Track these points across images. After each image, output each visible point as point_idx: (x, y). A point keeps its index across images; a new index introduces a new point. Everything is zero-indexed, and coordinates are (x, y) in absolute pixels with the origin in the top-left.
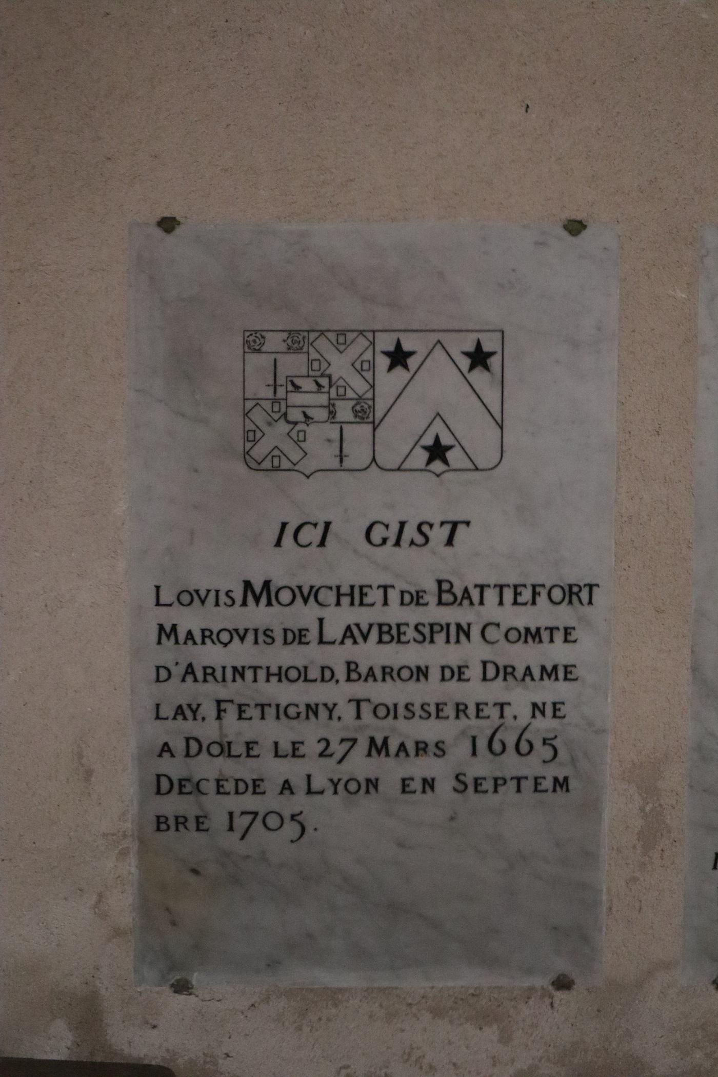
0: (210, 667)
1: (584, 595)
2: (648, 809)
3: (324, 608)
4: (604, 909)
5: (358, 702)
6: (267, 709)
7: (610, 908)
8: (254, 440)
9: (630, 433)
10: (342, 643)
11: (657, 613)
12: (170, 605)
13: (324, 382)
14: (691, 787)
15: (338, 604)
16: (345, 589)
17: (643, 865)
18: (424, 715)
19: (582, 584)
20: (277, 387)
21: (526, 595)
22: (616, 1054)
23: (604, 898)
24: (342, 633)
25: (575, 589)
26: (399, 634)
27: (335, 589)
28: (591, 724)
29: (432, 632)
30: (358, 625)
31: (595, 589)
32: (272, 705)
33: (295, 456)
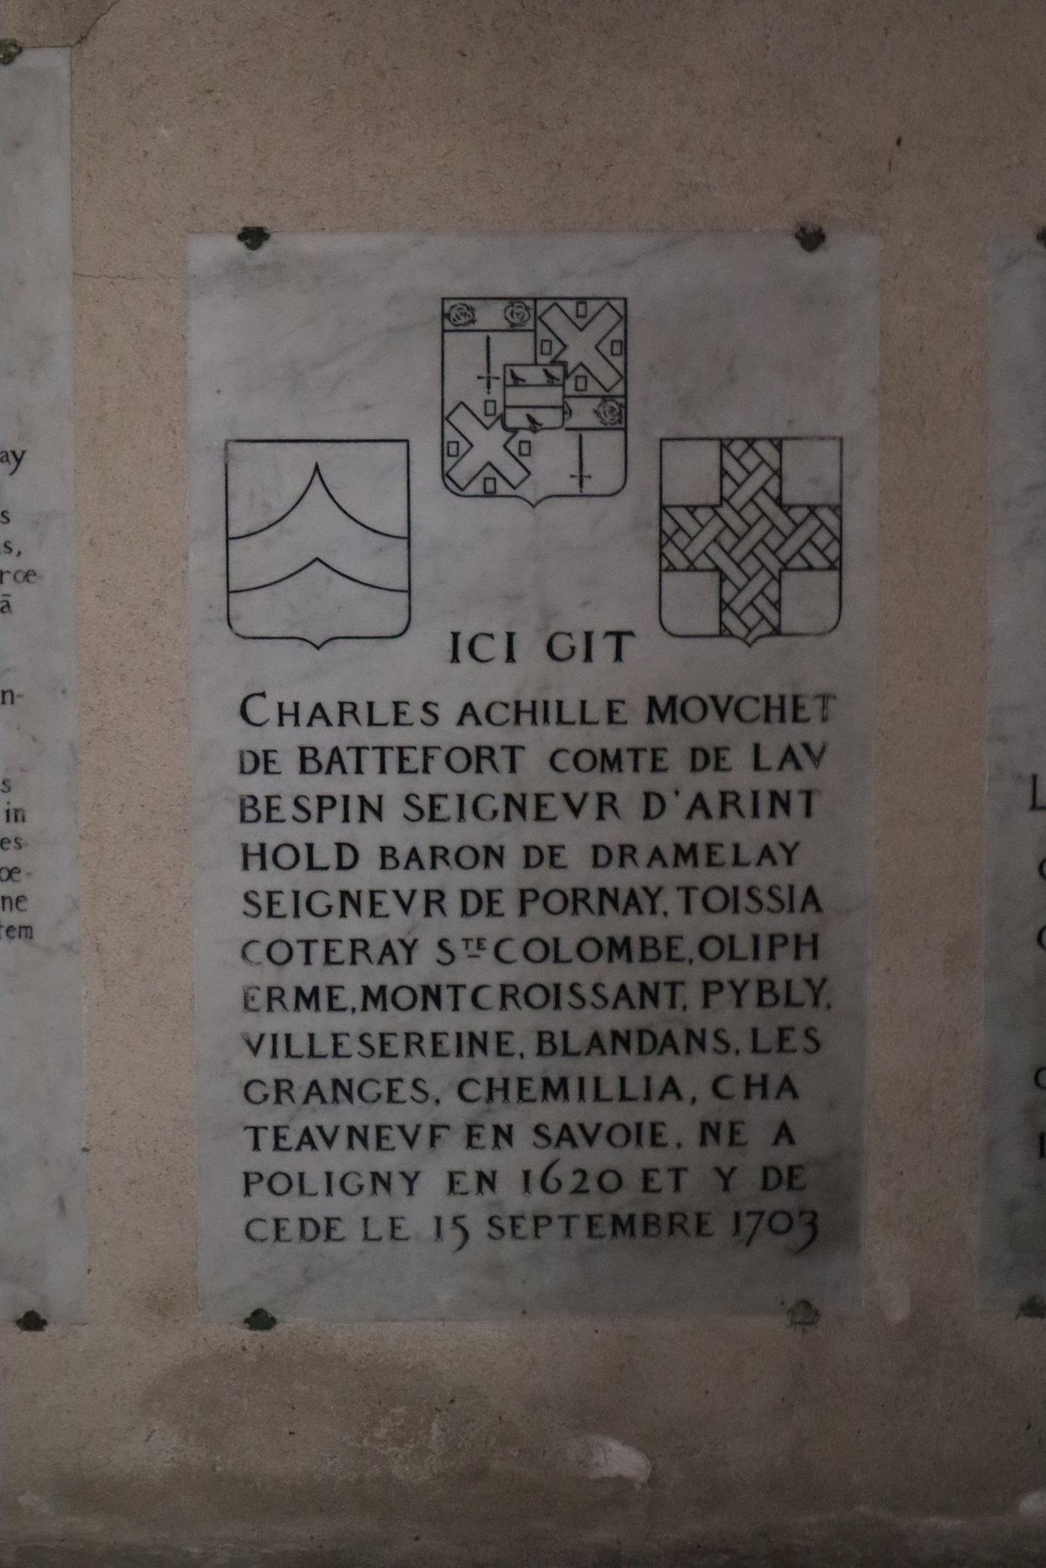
0: (389, 847)
5: (256, 1129)
8: (458, 455)
13: (557, 372)
18: (599, 1002)
20: (584, 479)
21: (416, 759)
26: (270, 808)
33: (515, 473)
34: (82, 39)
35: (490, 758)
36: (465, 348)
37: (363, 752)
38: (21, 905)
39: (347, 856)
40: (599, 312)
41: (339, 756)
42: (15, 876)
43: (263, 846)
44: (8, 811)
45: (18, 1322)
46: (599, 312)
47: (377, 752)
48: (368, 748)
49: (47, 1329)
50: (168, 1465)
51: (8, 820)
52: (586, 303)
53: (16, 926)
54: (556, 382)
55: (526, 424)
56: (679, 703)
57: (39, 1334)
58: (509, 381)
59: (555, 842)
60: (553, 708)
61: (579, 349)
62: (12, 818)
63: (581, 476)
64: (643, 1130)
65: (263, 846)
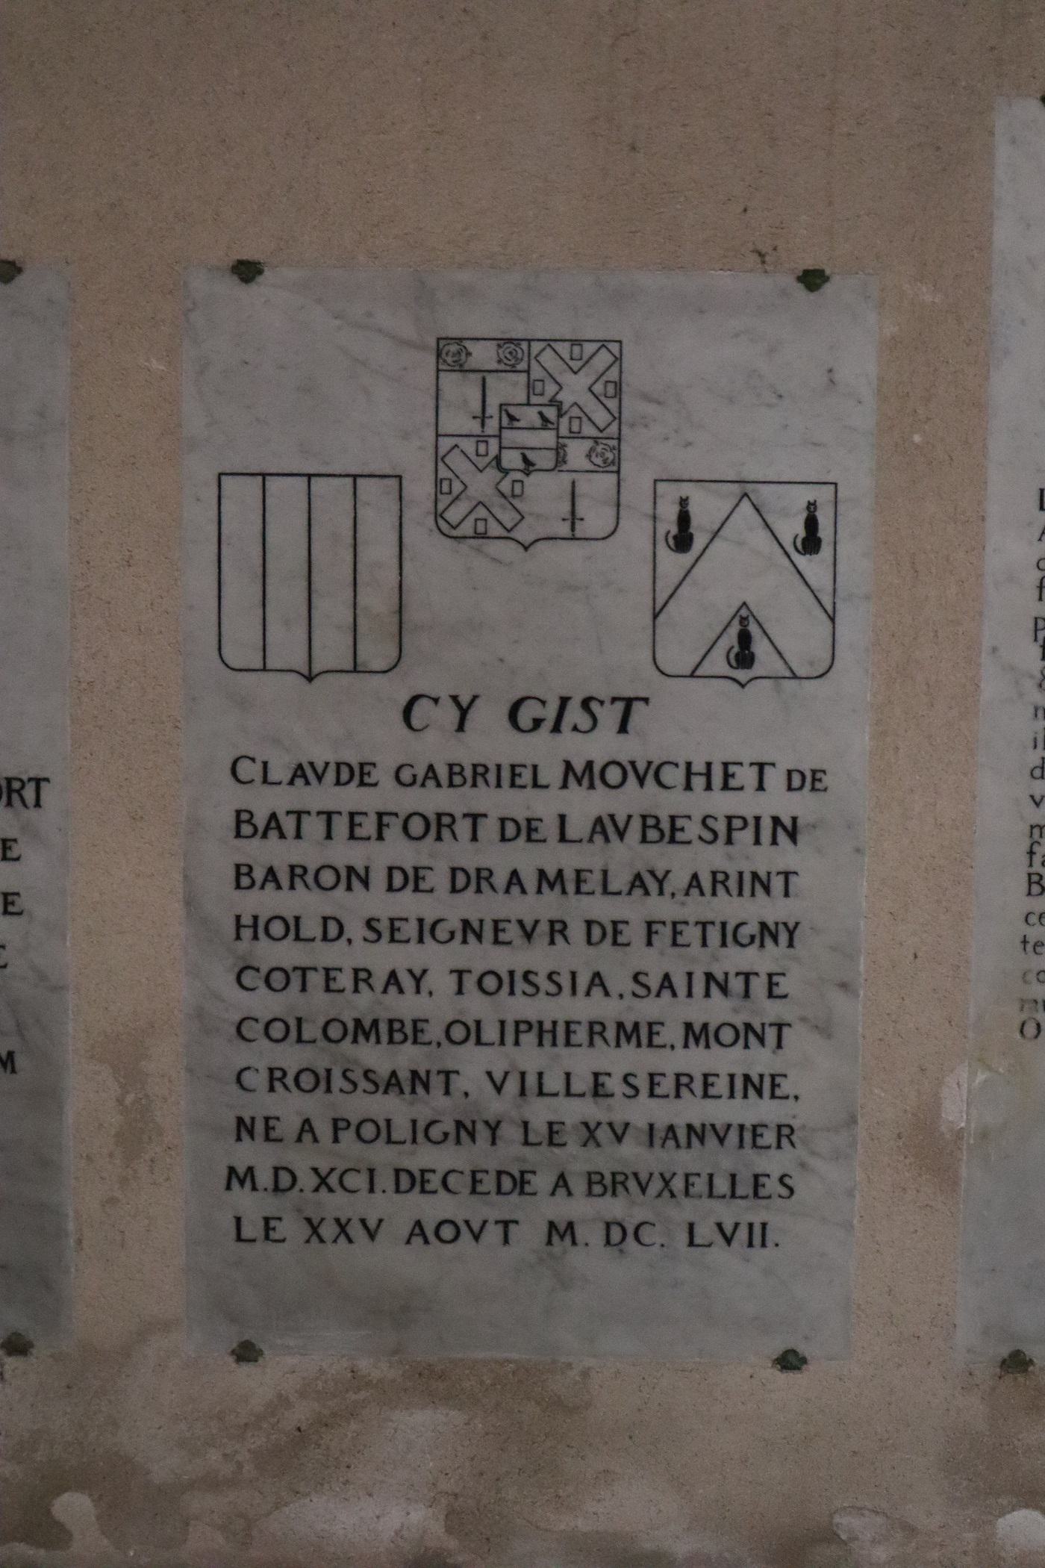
1: (29, 793)
2: (130, 1098)
3: (672, 790)
4: (72, 1242)
6: (709, 928)
7: (79, 1242)
9: (88, 563)
10: (591, 840)
11: (133, 821)
14: (190, 1070)
15: (688, 787)
16: (699, 767)
17: (124, 1181)
19: (25, 778)
21: (369, 827)
22: (94, 1450)
23: (71, 1226)
24: (589, 830)
25: (16, 785)
27: (683, 767)
28: (42, 977)
29: (730, 829)
30: (612, 817)
31: (43, 784)
32: (667, 923)
36: (461, 391)
37: (305, 818)
39: (333, 929)
40: (594, 354)
41: (277, 821)
43: (256, 918)
46: (594, 354)
48: (309, 813)
52: (581, 345)
54: (550, 426)
55: (521, 465)
56: (597, 769)
58: (505, 421)
59: (617, 917)
60: (311, 778)
61: (575, 389)
64: (760, 1241)
65: (256, 918)
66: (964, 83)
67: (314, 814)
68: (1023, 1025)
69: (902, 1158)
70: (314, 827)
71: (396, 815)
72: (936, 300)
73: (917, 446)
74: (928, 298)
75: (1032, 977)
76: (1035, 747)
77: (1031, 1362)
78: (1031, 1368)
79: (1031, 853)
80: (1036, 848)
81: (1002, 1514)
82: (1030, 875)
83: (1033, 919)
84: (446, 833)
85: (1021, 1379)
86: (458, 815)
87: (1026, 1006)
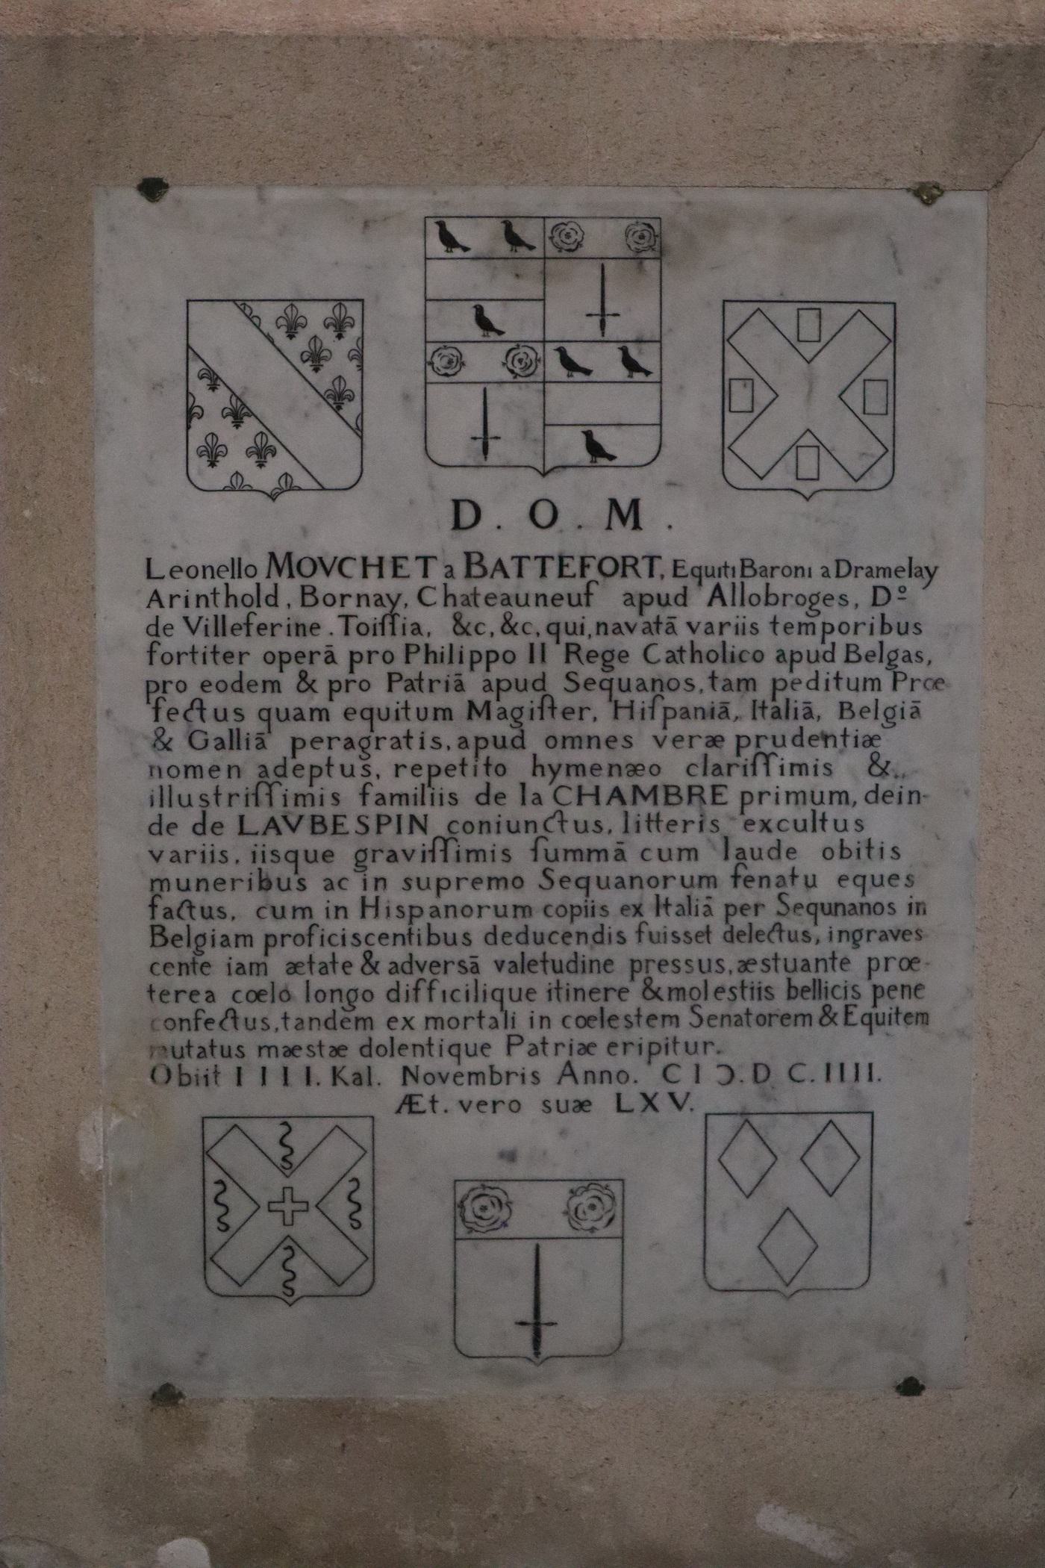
12: (163, 578)
34: (998, 184)
35: (633, 566)
38: (919, 993)
42: (915, 966)
44: (910, 905)
45: (898, 1388)
47: (539, 562)
49: (924, 1393)
50: (1028, 1521)
51: (910, 912)
53: (914, 1013)
57: (916, 1399)
62: (914, 911)
63: (603, 313)
66: (63, 176)
67: (532, 558)
68: (154, 1071)
69: (44, 1200)
70: (532, 569)
71: (594, 557)
72: (42, 382)
73: (27, 521)
74: (33, 380)
75: (160, 1024)
76: (152, 805)
77: (181, 1395)
78: (181, 1401)
79: (153, 906)
80: (157, 901)
81: (163, 1542)
82: (153, 927)
83: (158, 969)
84: (629, 571)
85: (173, 1412)
86: (640, 558)
87: (156, 1053)
